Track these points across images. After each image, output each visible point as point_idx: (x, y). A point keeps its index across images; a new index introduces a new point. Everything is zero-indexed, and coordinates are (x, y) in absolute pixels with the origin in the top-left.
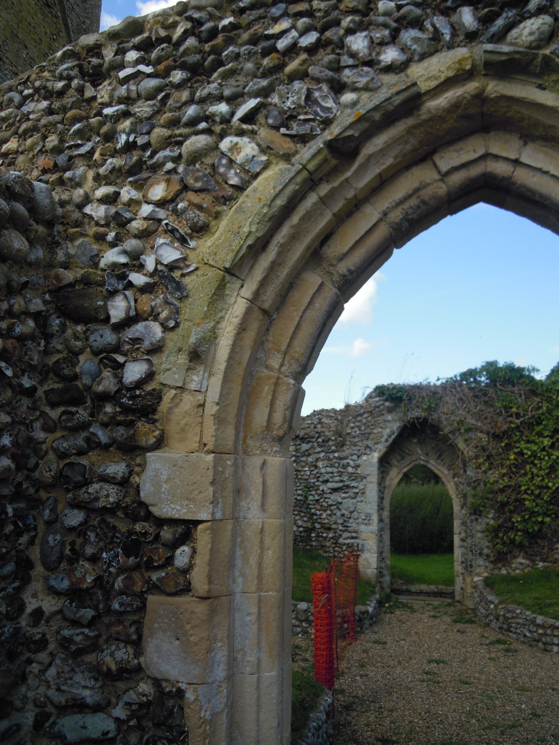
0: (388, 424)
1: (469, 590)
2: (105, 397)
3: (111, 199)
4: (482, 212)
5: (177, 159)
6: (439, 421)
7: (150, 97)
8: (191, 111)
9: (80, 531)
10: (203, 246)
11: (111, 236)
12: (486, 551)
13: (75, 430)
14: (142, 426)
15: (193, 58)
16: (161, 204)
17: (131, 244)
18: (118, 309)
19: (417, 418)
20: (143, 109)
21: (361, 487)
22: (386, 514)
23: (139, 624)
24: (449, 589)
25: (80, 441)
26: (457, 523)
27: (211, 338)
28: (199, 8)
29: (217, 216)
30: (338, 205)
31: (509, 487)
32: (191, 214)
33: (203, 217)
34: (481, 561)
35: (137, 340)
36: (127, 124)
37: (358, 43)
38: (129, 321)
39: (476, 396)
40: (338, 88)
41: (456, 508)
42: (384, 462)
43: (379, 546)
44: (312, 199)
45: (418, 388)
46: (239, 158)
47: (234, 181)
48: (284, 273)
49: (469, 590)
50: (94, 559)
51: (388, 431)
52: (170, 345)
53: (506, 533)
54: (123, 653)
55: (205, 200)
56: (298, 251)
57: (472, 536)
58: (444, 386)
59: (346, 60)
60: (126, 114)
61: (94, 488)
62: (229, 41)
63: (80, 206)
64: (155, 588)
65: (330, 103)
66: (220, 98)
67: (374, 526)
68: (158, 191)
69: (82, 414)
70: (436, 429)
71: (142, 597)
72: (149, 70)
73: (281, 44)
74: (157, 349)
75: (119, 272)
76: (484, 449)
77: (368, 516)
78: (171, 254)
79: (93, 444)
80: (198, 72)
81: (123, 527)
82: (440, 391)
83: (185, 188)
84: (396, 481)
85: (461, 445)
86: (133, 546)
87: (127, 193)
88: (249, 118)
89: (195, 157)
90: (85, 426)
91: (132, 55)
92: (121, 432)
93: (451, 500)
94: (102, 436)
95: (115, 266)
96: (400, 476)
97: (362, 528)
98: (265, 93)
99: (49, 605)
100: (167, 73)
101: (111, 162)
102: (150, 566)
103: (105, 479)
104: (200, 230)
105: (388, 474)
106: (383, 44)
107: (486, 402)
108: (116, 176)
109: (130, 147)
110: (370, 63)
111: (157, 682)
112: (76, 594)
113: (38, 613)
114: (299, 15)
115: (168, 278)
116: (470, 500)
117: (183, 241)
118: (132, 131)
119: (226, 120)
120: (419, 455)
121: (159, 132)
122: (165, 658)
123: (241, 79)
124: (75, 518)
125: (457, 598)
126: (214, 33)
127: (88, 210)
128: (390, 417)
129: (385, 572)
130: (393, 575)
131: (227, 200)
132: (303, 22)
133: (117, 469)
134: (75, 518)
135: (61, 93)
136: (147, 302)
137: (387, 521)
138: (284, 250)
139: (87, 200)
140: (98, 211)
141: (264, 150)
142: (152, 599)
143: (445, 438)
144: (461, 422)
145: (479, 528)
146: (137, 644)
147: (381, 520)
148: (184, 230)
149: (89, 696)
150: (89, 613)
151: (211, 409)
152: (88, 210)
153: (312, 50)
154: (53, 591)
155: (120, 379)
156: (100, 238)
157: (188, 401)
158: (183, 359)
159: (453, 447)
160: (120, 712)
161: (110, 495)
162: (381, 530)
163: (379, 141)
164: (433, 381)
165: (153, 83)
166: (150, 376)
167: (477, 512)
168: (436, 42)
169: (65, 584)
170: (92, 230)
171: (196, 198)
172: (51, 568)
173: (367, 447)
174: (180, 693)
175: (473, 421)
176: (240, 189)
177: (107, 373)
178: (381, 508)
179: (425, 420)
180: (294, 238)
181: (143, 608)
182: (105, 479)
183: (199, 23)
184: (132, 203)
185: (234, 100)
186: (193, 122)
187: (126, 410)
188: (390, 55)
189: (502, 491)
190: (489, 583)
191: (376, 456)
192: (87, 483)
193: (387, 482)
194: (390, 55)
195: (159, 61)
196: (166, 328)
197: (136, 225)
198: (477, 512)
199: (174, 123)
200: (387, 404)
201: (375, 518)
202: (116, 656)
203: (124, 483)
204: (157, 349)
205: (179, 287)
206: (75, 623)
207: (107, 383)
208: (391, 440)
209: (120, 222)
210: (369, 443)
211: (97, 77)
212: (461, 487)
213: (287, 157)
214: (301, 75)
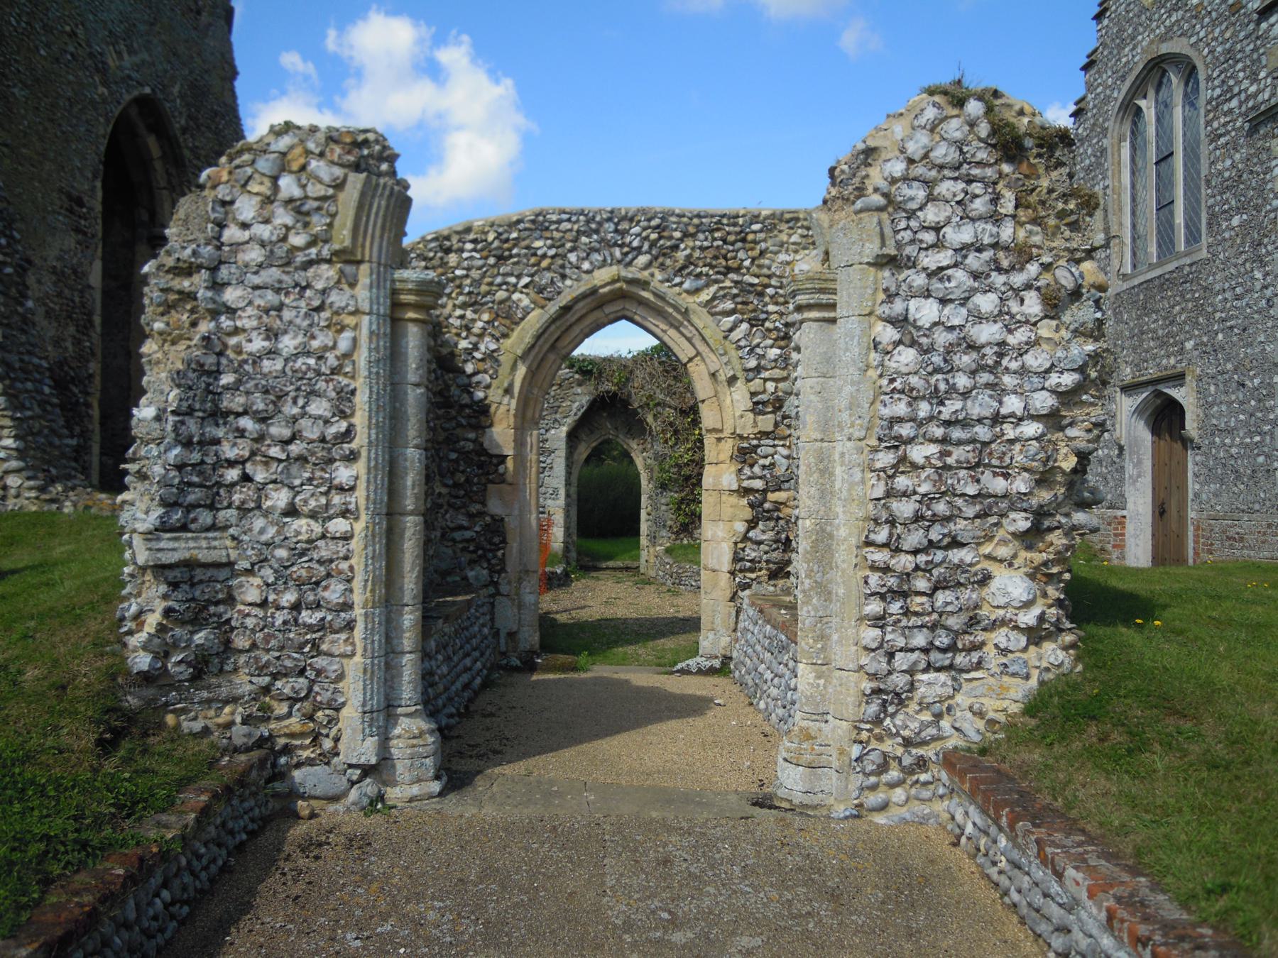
0: (578, 398)
1: (652, 560)
2: (466, 406)
3: (462, 317)
4: (624, 322)
5: (493, 302)
6: (629, 395)
7: (479, 268)
8: (499, 280)
9: (456, 461)
10: (507, 343)
11: (464, 334)
12: (669, 523)
13: (450, 420)
14: (483, 418)
15: (499, 252)
16: (487, 322)
17: (473, 339)
18: (469, 368)
19: (608, 392)
20: (475, 274)
21: (549, 461)
22: (573, 490)
23: (484, 496)
24: (635, 564)
25: (454, 424)
26: (644, 498)
27: (511, 385)
28: (500, 226)
29: (513, 330)
30: (564, 328)
31: (693, 461)
32: (502, 328)
33: (506, 330)
34: (664, 533)
35: (478, 383)
36: (468, 281)
37: (573, 257)
38: (475, 373)
39: (667, 372)
40: (564, 277)
41: (644, 482)
42: (573, 437)
43: (565, 522)
44: (553, 327)
45: (609, 360)
46: (522, 305)
47: (520, 316)
48: (541, 356)
49: (652, 560)
50: (463, 472)
51: (577, 404)
52: (494, 386)
53: (688, 505)
54: (478, 507)
55: (507, 322)
56: (547, 346)
57: (657, 509)
58: (635, 360)
59: (568, 265)
60: (467, 276)
61: (462, 443)
62: (515, 246)
63: (447, 319)
64: (492, 482)
65: (560, 284)
66: (512, 275)
67: (561, 501)
68: (486, 317)
69: (453, 413)
70: (626, 403)
71: (485, 485)
72: (478, 256)
73: (540, 252)
74: (488, 387)
75: (469, 352)
76: (671, 424)
77: (555, 491)
78: (493, 346)
79: (460, 425)
80: (501, 259)
81: (476, 458)
82: (630, 364)
83: (498, 315)
84: (585, 456)
85: (650, 419)
86: (480, 466)
87: (469, 314)
88: (526, 286)
89: (501, 302)
90: (455, 418)
91: (469, 246)
92: (473, 421)
93: (638, 474)
94: (464, 422)
95: (466, 349)
96: (589, 451)
97: (549, 502)
98: (532, 275)
99: (444, 491)
100: (486, 258)
101: (461, 298)
102: (488, 473)
103: (467, 440)
104: (505, 336)
105: (576, 448)
106: (583, 259)
107: (675, 377)
108: (464, 306)
109: (470, 293)
110: (578, 268)
111: (492, 517)
112: (456, 485)
113: (440, 494)
114: (547, 238)
115: (491, 356)
116: (656, 475)
117: (497, 340)
118: (471, 286)
119: (515, 285)
120: (608, 429)
121: (484, 288)
122: (495, 507)
123: (521, 266)
124: (454, 456)
125: (642, 571)
126: (507, 240)
127: (451, 320)
128: (579, 390)
129: (571, 547)
130: (579, 553)
131: (517, 324)
132: (549, 242)
133: (472, 435)
134: (454, 456)
135: (431, 259)
136: (481, 366)
137: (575, 496)
138: (541, 347)
139: (450, 316)
140: (457, 323)
141: (533, 302)
142: (490, 486)
143: (635, 412)
144: (650, 397)
145: (663, 501)
146: (484, 504)
147: (568, 495)
148: (498, 335)
149: (465, 523)
150: (462, 493)
151: (512, 412)
152: (451, 320)
153: (553, 257)
154: (446, 485)
155: (472, 398)
156: (458, 335)
157: (503, 409)
158: (500, 391)
159: (642, 422)
160: (477, 529)
161: (470, 446)
162: (568, 505)
163: (581, 304)
164: (624, 354)
165: (480, 263)
166: (486, 398)
167: (663, 486)
168: (604, 264)
169: (451, 482)
170: (454, 331)
171: (504, 321)
172: (442, 476)
173: (556, 420)
174: (502, 519)
175: (661, 396)
176: (522, 319)
177: (465, 395)
178: (568, 483)
179: (615, 394)
180: (545, 342)
181: (485, 490)
182: (467, 440)
183: (500, 234)
184: (474, 321)
185: (519, 277)
186: (500, 285)
187: (475, 411)
188: (586, 266)
189: (687, 465)
190: (668, 551)
191: (565, 429)
192: (458, 442)
193: (575, 457)
194: (586, 266)
195: (482, 250)
196: (492, 378)
197: (476, 330)
198: (663, 486)
199: (491, 284)
200: (577, 376)
201: (562, 492)
202: (475, 508)
203: (474, 441)
204: (488, 387)
205: (497, 360)
206: (457, 497)
207: (465, 399)
208: (580, 414)
209: (468, 329)
210: (558, 416)
211: (448, 251)
212: (649, 461)
213: (543, 307)
214: (548, 269)
